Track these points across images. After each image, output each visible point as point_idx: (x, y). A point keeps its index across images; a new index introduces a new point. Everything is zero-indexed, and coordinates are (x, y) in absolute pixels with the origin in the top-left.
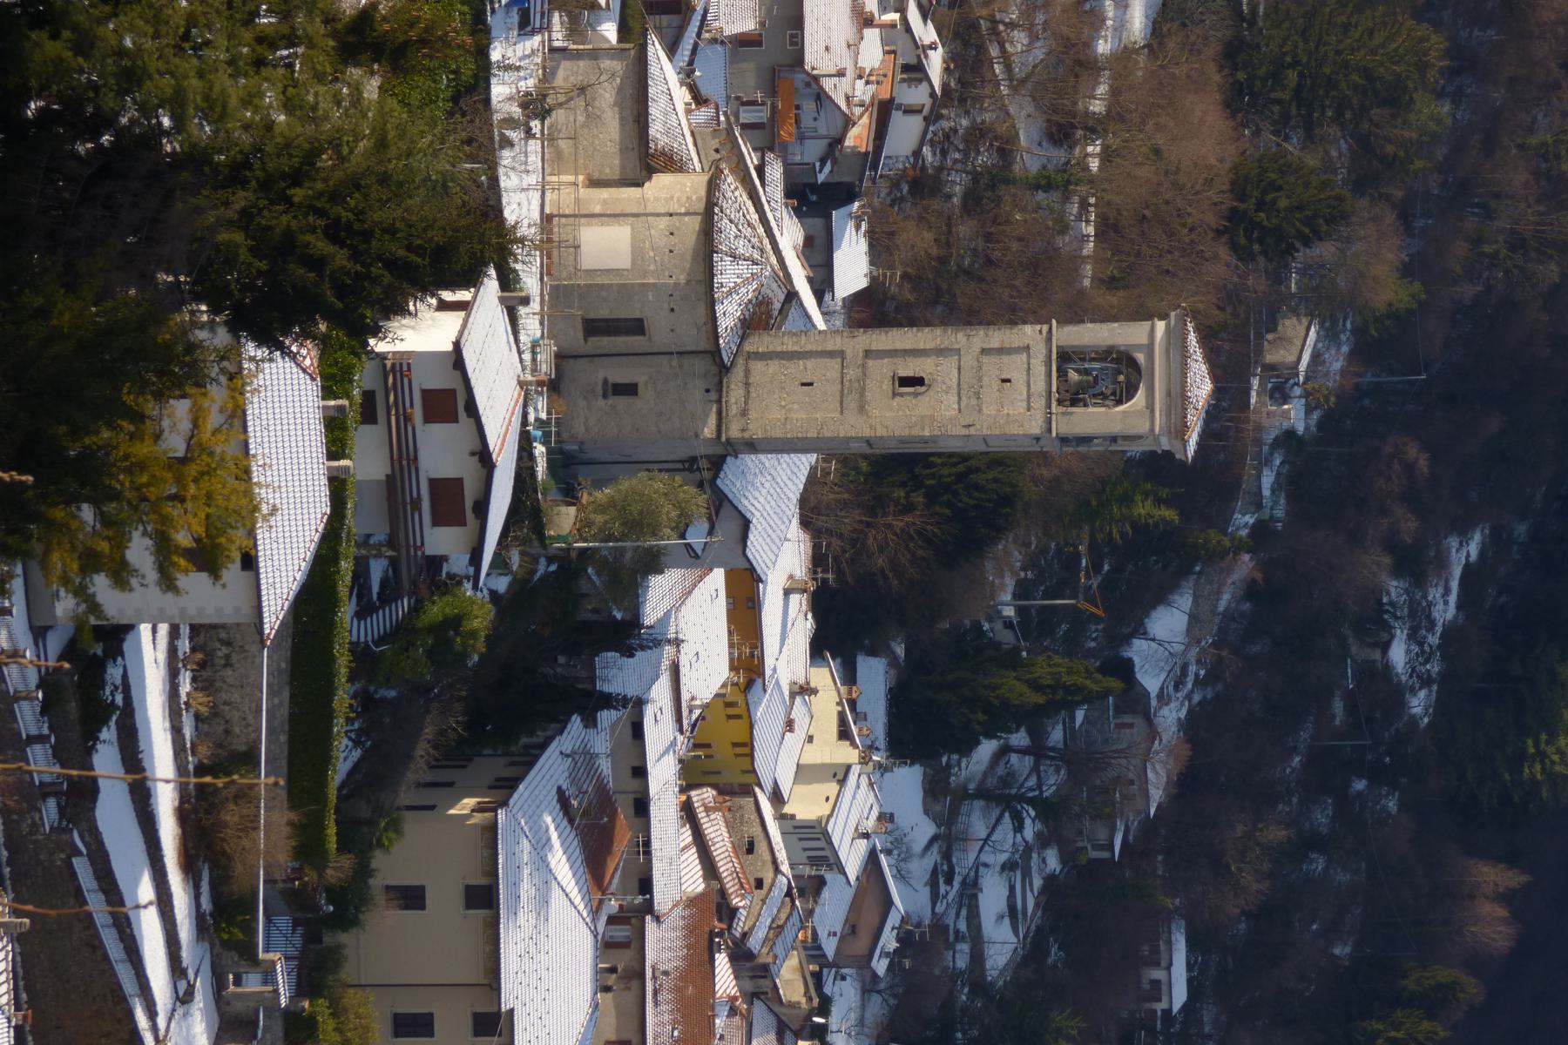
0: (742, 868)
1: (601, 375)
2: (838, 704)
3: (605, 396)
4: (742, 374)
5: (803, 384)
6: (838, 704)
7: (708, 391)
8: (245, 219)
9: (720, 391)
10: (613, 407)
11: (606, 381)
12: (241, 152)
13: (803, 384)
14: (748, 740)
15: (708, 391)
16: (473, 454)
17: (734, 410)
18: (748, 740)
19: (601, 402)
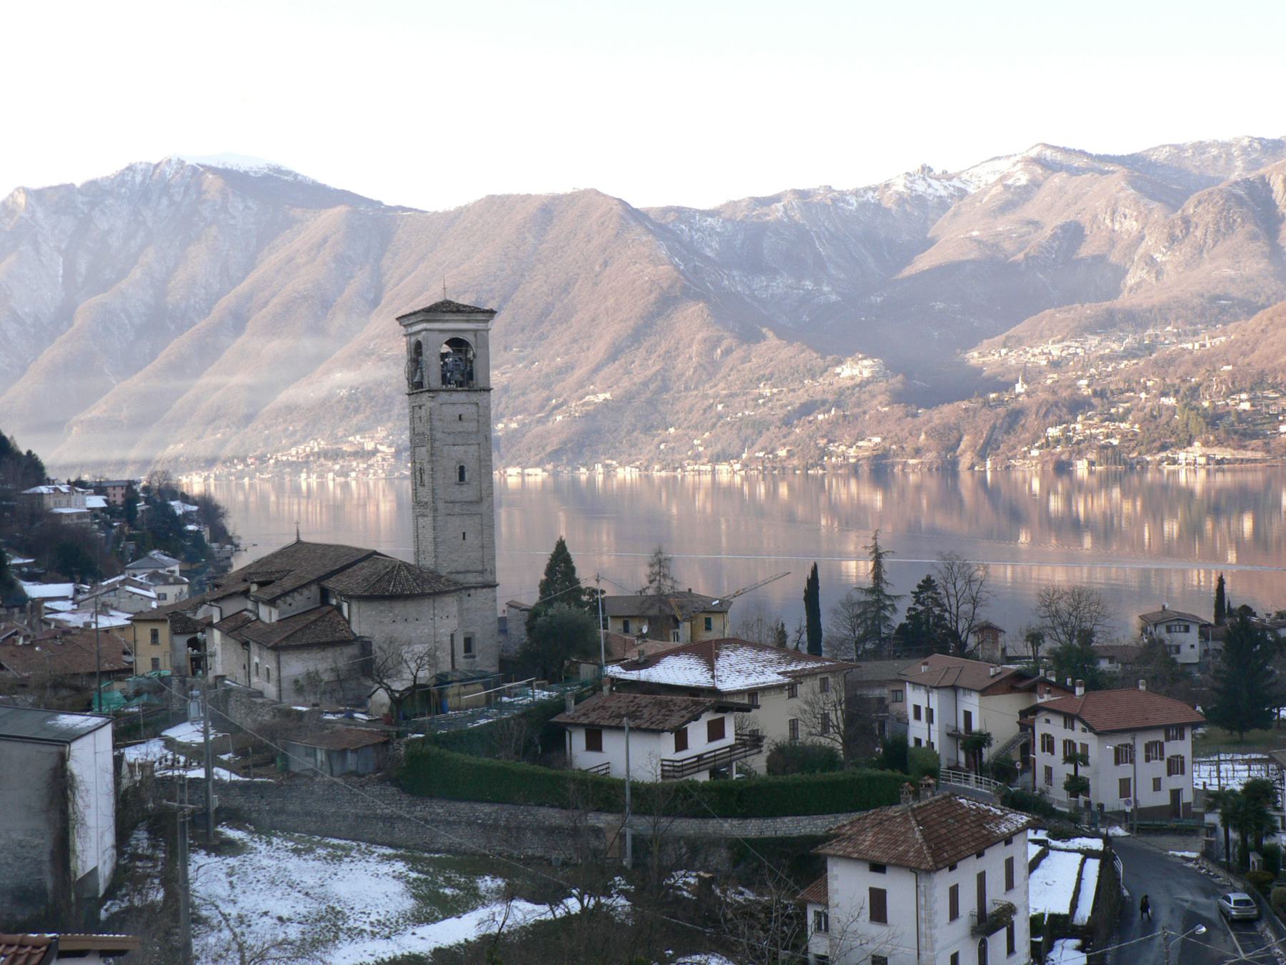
0: (391, 846)
1: (462, 660)
2: (945, 172)
3: (474, 657)
4: (460, 575)
5: (464, 538)
6: (945, 172)
7: (469, 595)
8: (1192, 919)
9: (469, 588)
10: (480, 652)
11: (465, 657)
12: (1136, 333)
13: (464, 538)
14: (622, 620)
15: (469, 595)
16: (690, 590)
17: (480, 579)
18: (622, 620)
19: (477, 659)
